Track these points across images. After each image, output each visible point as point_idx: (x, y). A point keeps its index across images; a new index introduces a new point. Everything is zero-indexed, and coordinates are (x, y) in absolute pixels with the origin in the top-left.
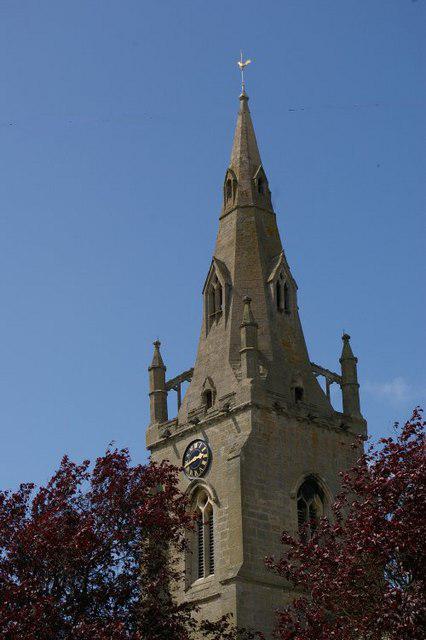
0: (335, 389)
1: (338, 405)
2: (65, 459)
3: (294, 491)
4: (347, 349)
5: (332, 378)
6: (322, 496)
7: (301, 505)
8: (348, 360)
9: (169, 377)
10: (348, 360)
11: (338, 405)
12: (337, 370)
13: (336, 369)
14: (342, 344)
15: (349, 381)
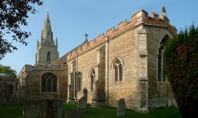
6: (51, 53)
7: (48, 55)
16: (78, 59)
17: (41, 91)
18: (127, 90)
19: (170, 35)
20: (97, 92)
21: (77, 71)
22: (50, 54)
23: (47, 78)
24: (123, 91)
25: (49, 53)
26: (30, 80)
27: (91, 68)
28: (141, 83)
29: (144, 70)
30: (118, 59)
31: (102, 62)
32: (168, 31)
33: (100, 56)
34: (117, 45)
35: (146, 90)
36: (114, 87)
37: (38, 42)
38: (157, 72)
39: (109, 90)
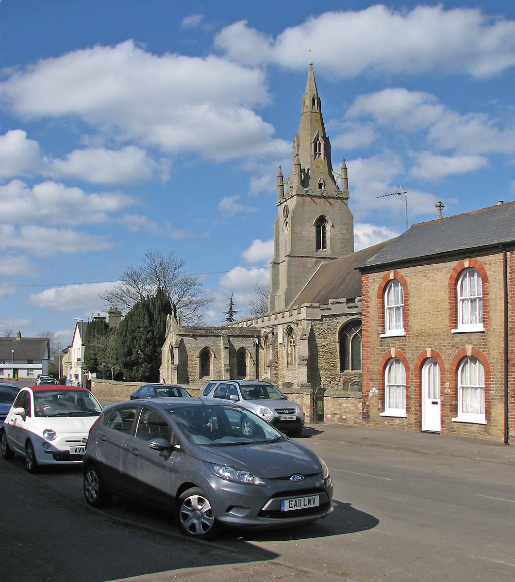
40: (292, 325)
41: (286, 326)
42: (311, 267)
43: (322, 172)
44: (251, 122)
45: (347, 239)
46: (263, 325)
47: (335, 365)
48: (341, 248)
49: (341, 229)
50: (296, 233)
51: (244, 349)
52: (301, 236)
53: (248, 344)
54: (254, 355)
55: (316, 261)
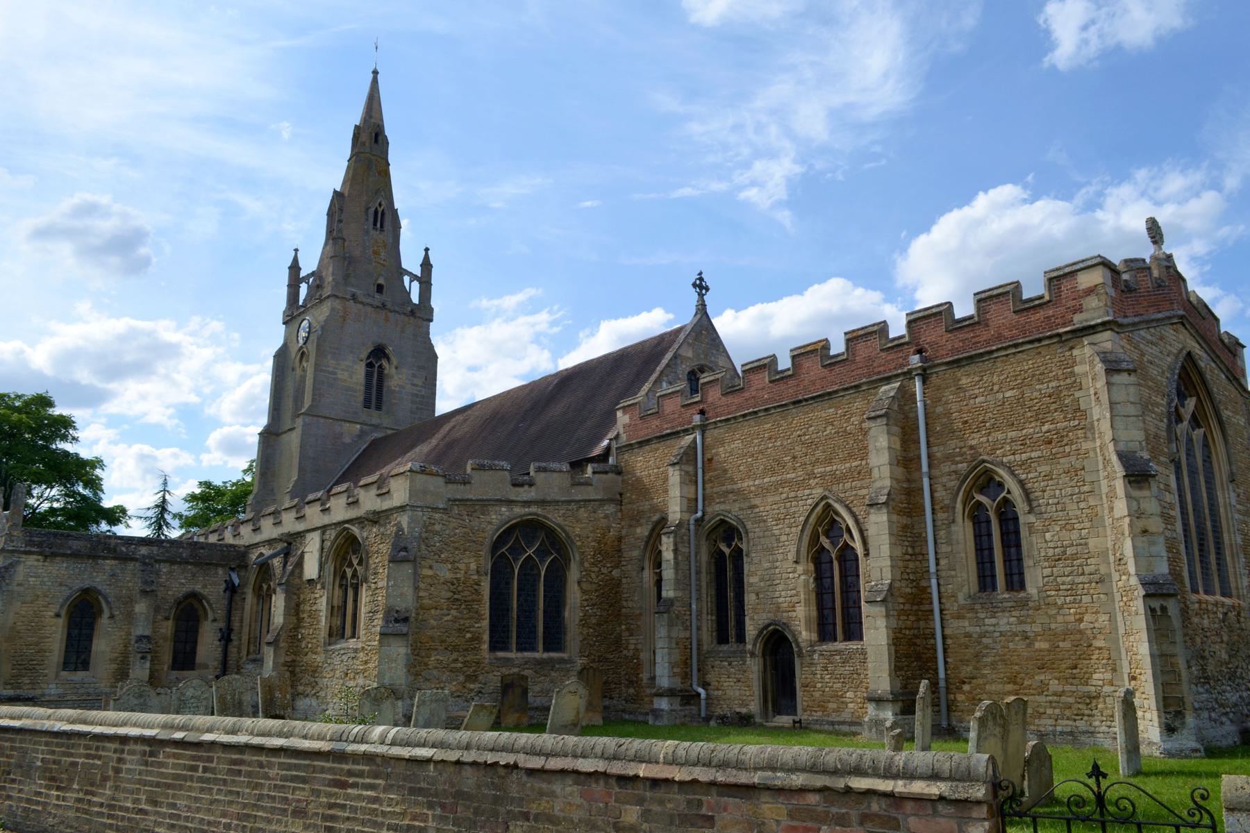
0: (416, 285)
1: (415, 298)
2: (700, 274)
3: (364, 355)
4: (426, 258)
5: (414, 278)
6: (388, 359)
7: (370, 365)
8: (426, 265)
9: (303, 274)
10: (426, 265)
11: (415, 298)
12: (417, 271)
13: (417, 271)
14: (424, 253)
15: (425, 281)
16: (708, 440)
17: (486, 646)
18: (1064, 640)
19: (1202, 353)
20: (893, 648)
21: (704, 514)
22: (384, 362)
23: (516, 550)
24: (1037, 645)
25: (379, 353)
26: (430, 573)
27: (817, 505)
28: (1153, 610)
29: (1152, 543)
30: (987, 471)
31: (896, 479)
32: (1188, 335)
33: (889, 448)
34: (977, 400)
35: (1174, 643)
36: (979, 622)
37: (295, 267)
38: (1182, 547)
39: (949, 641)
40: (355, 530)
41: (331, 534)
42: (350, 441)
43: (384, 266)
44: (176, 421)
45: (423, 397)
46: (258, 538)
47: (477, 638)
48: (412, 412)
49: (414, 376)
50: (325, 371)
51: (200, 602)
52: (335, 379)
53: (211, 587)
54: (221, 613)
55: (361, 431)
